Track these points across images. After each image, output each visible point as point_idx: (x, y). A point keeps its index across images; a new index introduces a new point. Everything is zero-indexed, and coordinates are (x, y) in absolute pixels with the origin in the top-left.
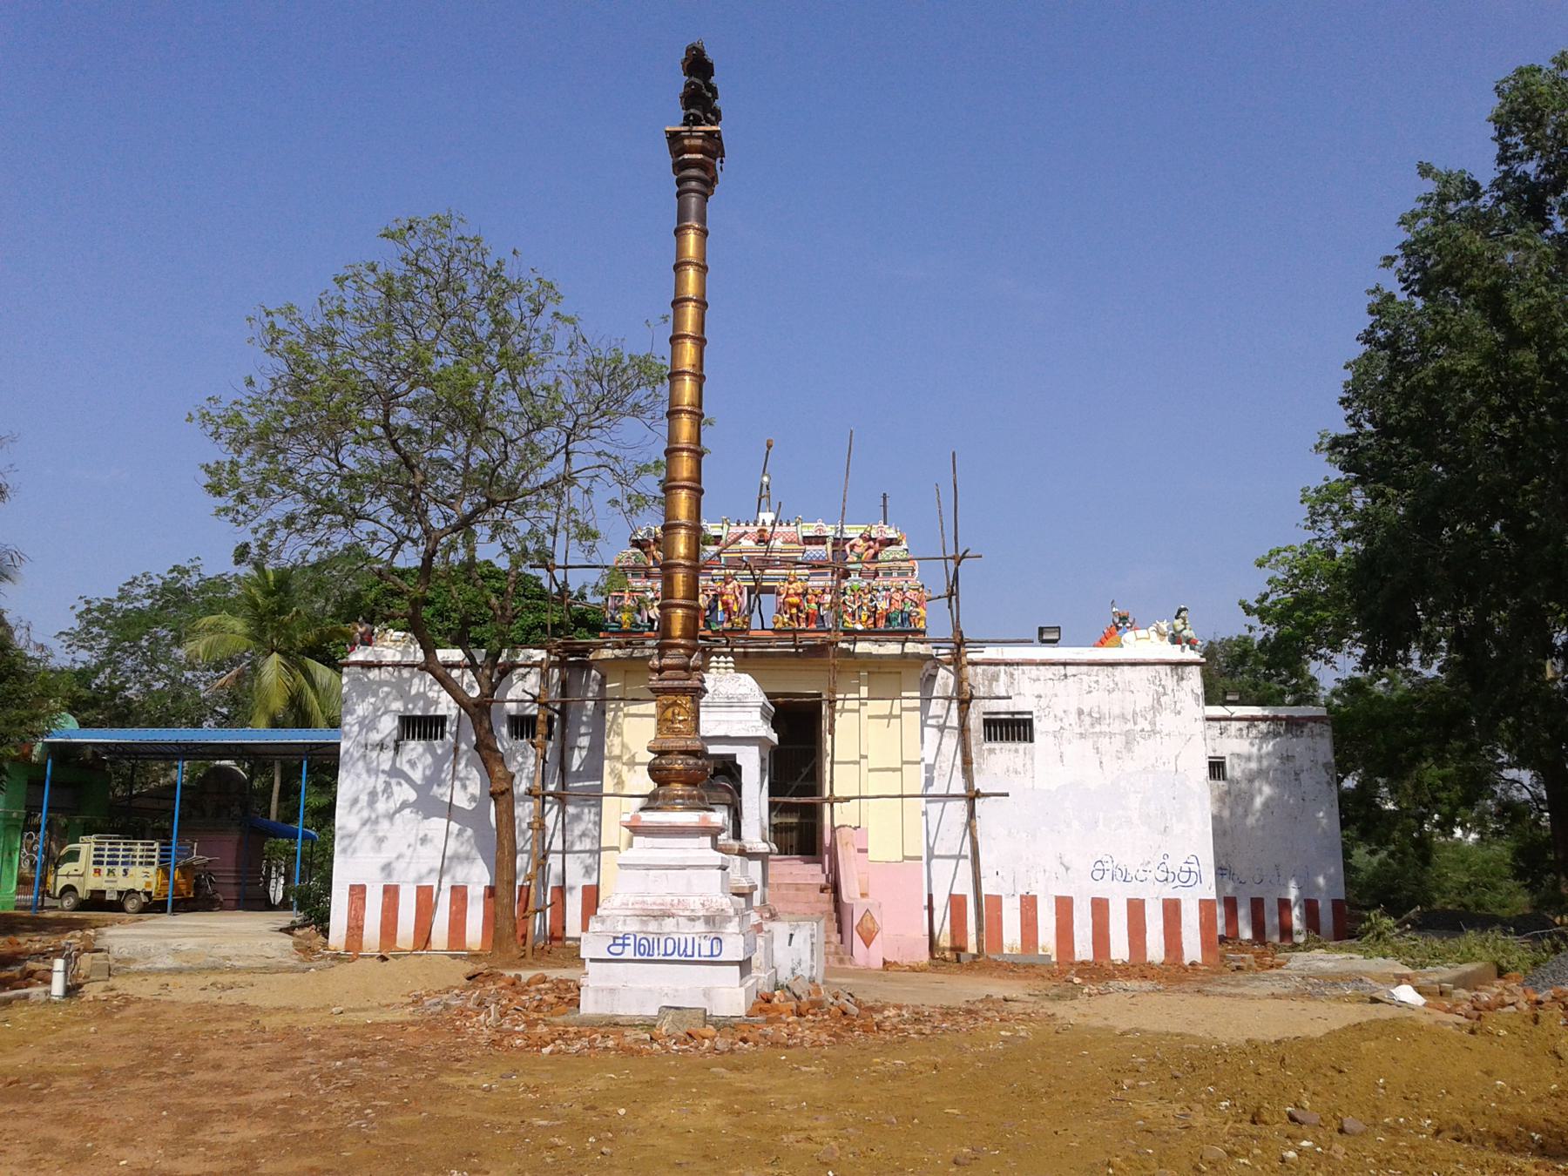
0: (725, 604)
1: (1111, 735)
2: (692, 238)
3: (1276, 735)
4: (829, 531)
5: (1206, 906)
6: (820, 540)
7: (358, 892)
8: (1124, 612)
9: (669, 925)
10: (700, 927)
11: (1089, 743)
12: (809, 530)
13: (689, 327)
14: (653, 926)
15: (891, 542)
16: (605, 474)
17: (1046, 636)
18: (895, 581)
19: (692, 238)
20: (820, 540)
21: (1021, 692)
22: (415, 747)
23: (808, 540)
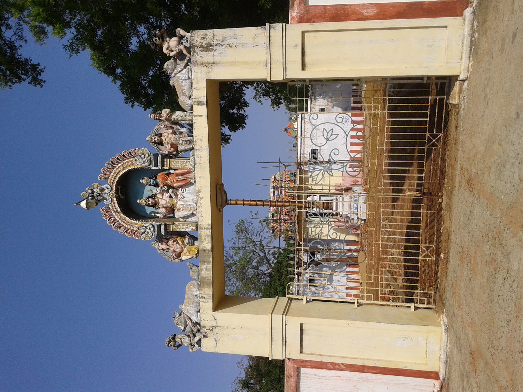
0: (288, 212)
1: (316, 133)
2: (232, 202)
3: (315, 96)
4: (272, 190)
5: (353, 115)
6: (274, 192)
7: (348, 295)
8: (284, 129)
9: (352, 205)
10: (352, 199)
11: (318, 138)
12: (272, 195)
13: (249, 203)
14: (352, 207)
15: (275, 177)
16: (261, 234)
17: (295, 146)
18: (283, 176)
19: (232, 202)
20: (274, 192)
21: (308, 151)
22: (317, 283)
23: (274, 194)
